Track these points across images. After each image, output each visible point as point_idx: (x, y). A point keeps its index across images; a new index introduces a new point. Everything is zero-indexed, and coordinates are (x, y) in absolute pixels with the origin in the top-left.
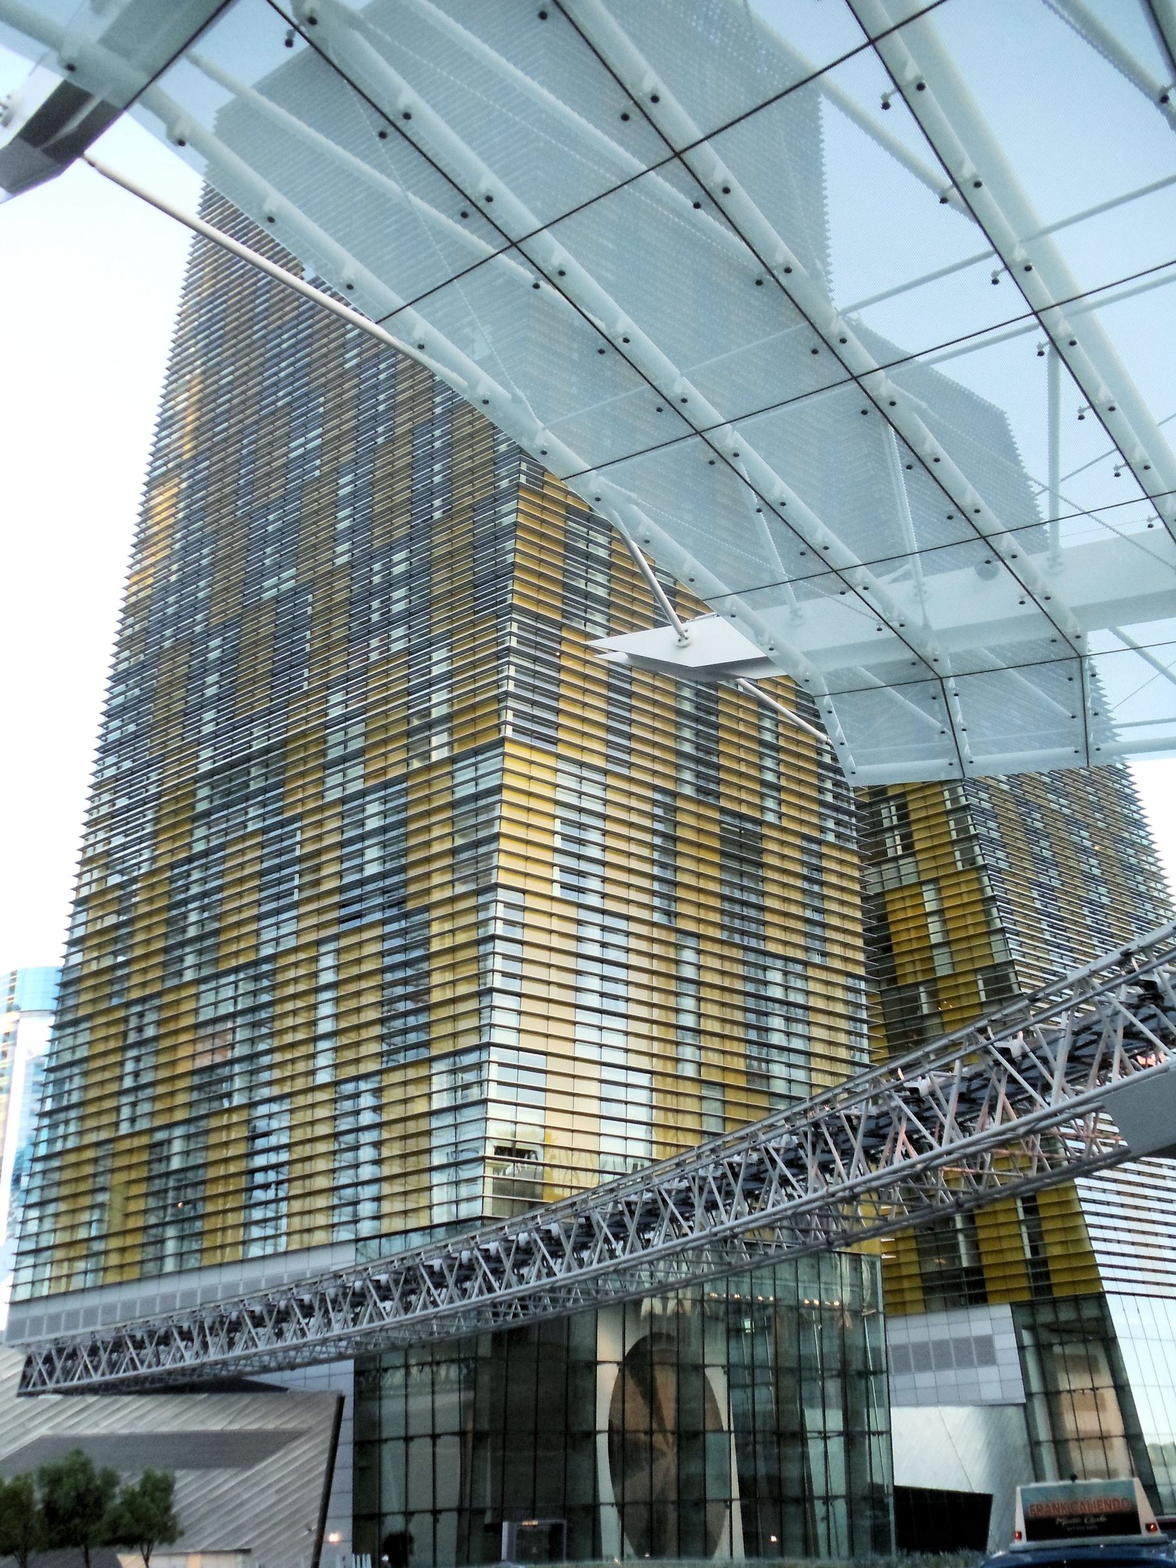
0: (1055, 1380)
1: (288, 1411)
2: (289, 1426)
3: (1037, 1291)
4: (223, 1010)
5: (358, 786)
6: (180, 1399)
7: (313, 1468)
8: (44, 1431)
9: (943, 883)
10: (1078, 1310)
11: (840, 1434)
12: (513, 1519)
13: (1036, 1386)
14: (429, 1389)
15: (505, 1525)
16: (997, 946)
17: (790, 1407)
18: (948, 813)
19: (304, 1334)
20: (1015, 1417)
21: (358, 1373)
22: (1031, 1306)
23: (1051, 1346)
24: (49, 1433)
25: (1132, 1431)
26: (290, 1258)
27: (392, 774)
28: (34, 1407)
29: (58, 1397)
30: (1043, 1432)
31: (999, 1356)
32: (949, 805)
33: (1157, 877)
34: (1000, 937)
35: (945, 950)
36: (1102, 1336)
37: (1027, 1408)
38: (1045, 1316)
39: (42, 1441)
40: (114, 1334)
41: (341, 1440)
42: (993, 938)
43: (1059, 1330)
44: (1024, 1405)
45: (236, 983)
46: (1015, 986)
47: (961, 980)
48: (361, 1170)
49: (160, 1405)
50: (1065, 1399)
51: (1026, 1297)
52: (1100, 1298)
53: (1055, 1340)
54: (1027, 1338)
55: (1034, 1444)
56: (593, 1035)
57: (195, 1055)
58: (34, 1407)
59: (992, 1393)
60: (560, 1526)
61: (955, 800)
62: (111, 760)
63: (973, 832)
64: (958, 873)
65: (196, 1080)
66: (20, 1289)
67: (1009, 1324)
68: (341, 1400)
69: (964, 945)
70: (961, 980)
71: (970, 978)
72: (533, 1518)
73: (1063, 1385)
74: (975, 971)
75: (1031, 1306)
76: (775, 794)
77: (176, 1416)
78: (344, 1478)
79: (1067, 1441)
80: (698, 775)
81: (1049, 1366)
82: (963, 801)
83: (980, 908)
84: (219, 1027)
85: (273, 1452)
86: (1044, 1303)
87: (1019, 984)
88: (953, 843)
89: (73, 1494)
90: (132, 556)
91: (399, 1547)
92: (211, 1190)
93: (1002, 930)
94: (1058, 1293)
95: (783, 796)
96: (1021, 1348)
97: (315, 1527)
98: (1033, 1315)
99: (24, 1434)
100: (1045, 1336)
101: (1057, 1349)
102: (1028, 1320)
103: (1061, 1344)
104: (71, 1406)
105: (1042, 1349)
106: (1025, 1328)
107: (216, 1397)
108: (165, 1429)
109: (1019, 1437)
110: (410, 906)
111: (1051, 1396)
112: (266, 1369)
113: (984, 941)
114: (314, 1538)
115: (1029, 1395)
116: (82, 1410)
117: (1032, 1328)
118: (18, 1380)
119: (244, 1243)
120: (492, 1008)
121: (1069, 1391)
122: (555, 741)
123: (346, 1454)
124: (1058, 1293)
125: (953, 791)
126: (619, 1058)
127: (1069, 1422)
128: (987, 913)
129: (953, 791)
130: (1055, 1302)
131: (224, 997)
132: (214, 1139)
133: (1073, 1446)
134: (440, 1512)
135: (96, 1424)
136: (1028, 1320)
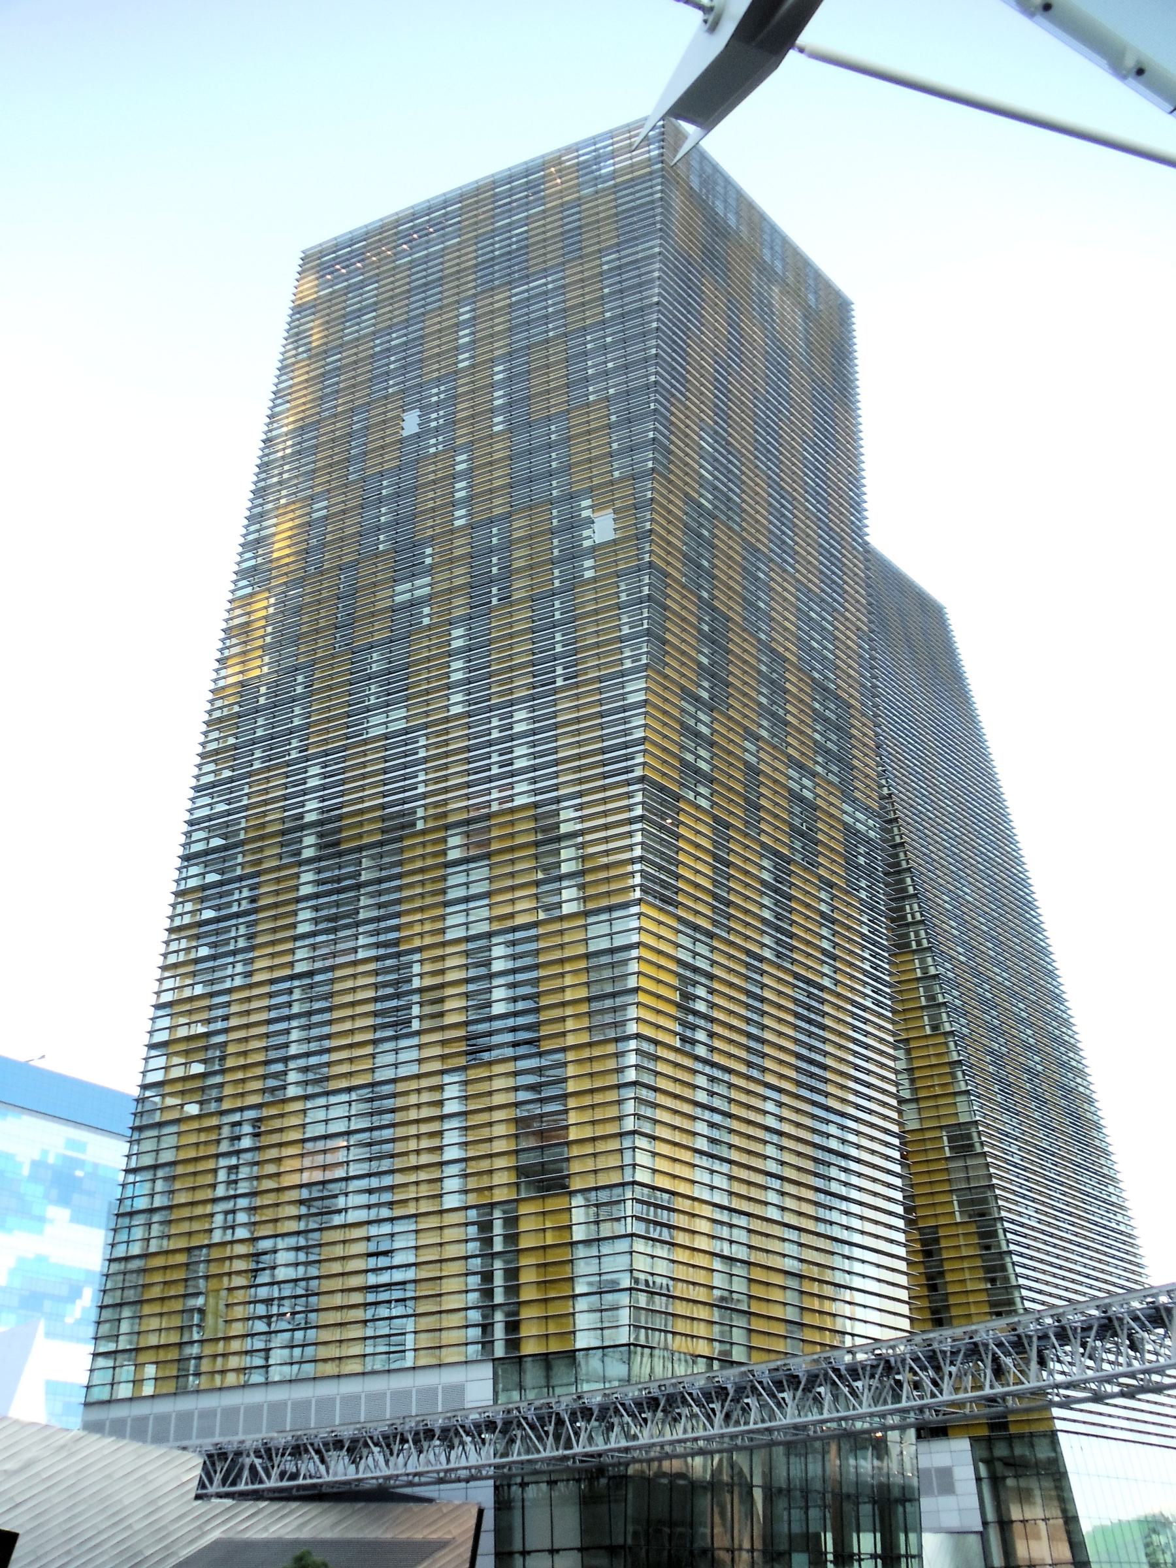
0: (1008, 1510)
8: (216, 1535)
9: (913, 1044)
10: (1011, 1447)
11: (874, 1556)
13: (991, 1516)
14: (527, 1504)
16: (962, 1107)
17: (702, 1530)
18: (918, 979)
19: (568, 1446)
20: (974, 1542)
21: (496, 1488)
22: (989, 1441)
23: (1004, 1478)
26: (419, 1373)
28: (211, 1510)
29: (229, 1502)
31: (959, 1487)
32: (919, 974)
33: (1074, 1048)
34: (964, 1098)
35: (914, 1106)
36: (1055, 1474)
37: (983, 1535)
38: (1001, 1451)
39: (216, 1543)
40: (235, 1445)
41: (480, 1551)
42: (959, 1099)
44: (981, 1533)
46: (978, 1145)
50: (1017, 1528)
51: (985, 1432)
52: (1052, 1436)
56: (705, 1178)
57: (300, 1171)
58: (211, 1510)
59: (953, 1522)
61: (925, 970)
62: (194, 870)
63: (941, 1000)
64: (926, 1036)
65: (305, 1194)
66: (95, 1390)
67: (968, 1457)
68: (481, 1512)
69: (932, 1103)
70: (928, 1135)
71: (936, 1134)
73: (1015, 1513)
74: (941, 1127)
76: (708, 940)
80: (778, 942)
82: (932, 971)
85: (423, 1560)
86: (999, 1439)
87: (982, 1144)
88: (922, 1008)
93: (967, 1092)
94: (1013, 1430)
95: (715, 944)
96: (979, 1479)
98: (990, 1449)
99: (204, 1534)
100: (1000, 1468)
101: (1010, 1482)
102: (984, 1454)
103: (1016, 1477)
105: (996, 1482)
106: (982, 1461)
107: (373, 1506)
108: (328, 1535)
110: (546, 1046)
111: (1005, 1525)
112: (411, 1484)
113: (950, 1100)
115: (985, 1524)
116: (253, 1515)
117: (989, 1462)
118: (196, 1482)
119: (223, 1355)
120: (634, 1148)
121: (1024, 1521)
124: (1013, 1430)
125: (922, 961)
126: (723, 1200)
128: (953, 1075)
129: (922, 961)
130: (1010, 1440)
131: (336, 1114)
132: (327, 1252)
135: (266, 1529)
136: (984, 1454)
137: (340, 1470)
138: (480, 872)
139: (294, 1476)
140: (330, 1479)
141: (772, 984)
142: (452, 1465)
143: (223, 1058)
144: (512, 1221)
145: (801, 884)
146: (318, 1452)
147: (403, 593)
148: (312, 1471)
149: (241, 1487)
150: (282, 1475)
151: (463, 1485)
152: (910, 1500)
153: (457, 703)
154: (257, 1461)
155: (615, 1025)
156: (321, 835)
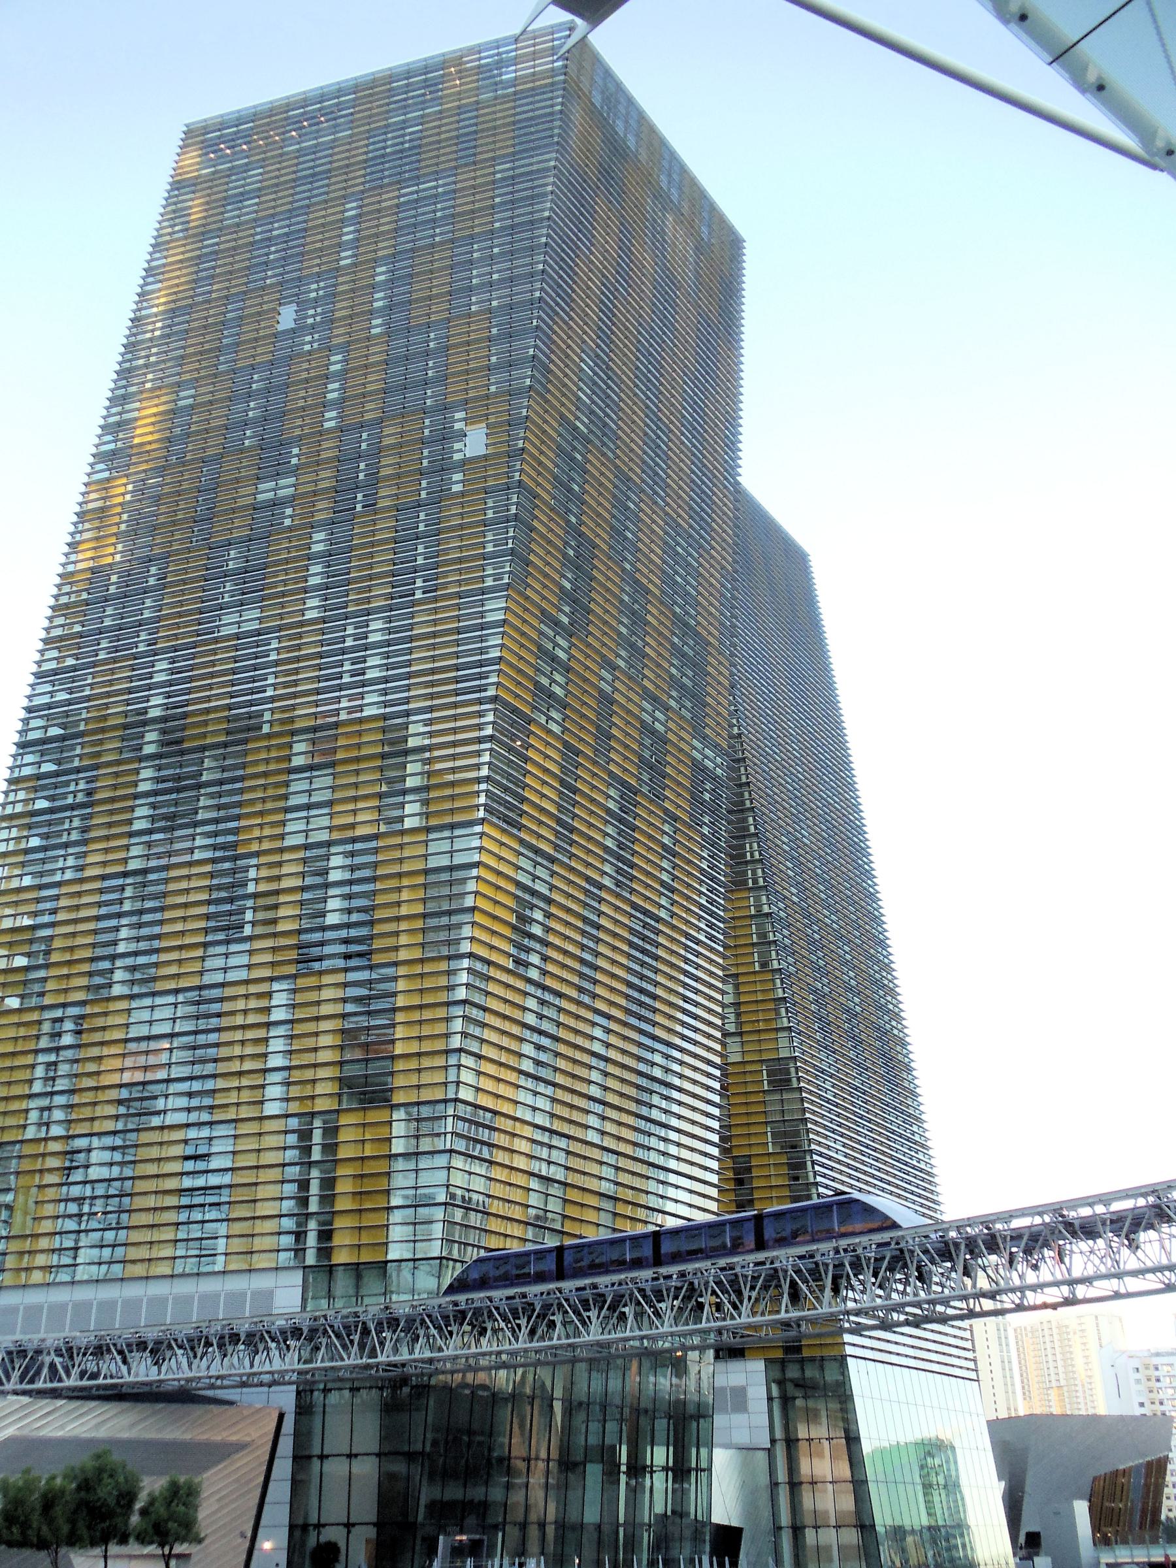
1: (145, 1419)
2: (234, 1438)
3: (787, 1350)
4: (157, 1030)
5: (324, 836)
6: (141, 1406)
7: (251, 1480)
8: (10, 1432)
12: (447, 1534)
13: (779, 1434)
15: (441, 1537)
16: (783, 1043)
18: (752, 917)
19: (373, 1354)
20: (762, 1456)
21: (298, 1393)
22: (783, 1363)
23: (794, 1398)
24: (17, 1433)
25: (858, 1477)
27: (360, 831)
29: (25, 1399)
30: (782, 1476)
31: (751, 1406)
34: (786, 1034)
35: (738, 1039)
37: (770, 1452)
38: (793, 1372)
43: (803, 1385)
45: (175, 1005)
47: (749, 1068)
48: (91, 1170)
49: (122, 1412)
50: (803, 1446)
51: (779, 1354)
52: (842, 1360)
53: (798, 1393)
54: (775, 1392)
55: (774, 1485)
56: (529, 1099)
59: (743, 1438)
60: (480, 1542)
61: (759, 907)
64: (755, 973)
65: (124, 1094)
68: (281, 1417)
70: (749, 1068)
72: (461, 1533)
73: (802, 1433)
74: (762, 1061)
75: (783, 1363)
77: (133, 1425)
78: (280, 1490)
79: (801, 1483)
80: (619, 871)
81: (791, 1414)
82: (766, 909)
83: (772, 1006)
84: (153, 1045)
85: (219, 1462)
88: (753, 944)
89: (115, 1493)
90: (66, 555)
91: (328, 1554)
92: (139, 1202)
94: (806, 1353)
96: (770, 1399)
97: (249, 1535)
98: (783, 1371)
100: (791, 1389)
101: (799, 1403)
103: (805, 1397)
104: (41, 1408)
105: (786, 1401)
109: (764, 1480)
111: (791, 1443)
114: (247, 1544)
116: (48, 1413)
121: (809, 1440)
122: (521, 827)
123: (283, 1468)
124: (806, 1353)
127: (805, 1468)
130: (802, 1361)
132: (143, 1153)
133: (805, 1488)
134: (354, 1525)
135: (62, 1427)
136: (777, 1375)
137: (142, 1371)
138: (323, 780)
139: (94, 1376)
140: (131, 1379)
141: (610, 914)
142: (255, 1370)
143: (47, 953)
144: (331, 1131)
145: (645, 815)
146: (121, 1352)
147: (266, 491)
148: (111, 1370)
149: (39, 1385)
150: (82, 1374)
151: (266, 1389)
152: (704, 1417)
153: (313, 609)
154: (58, 1360)
155: (449, 943)
156: (164, 732)
